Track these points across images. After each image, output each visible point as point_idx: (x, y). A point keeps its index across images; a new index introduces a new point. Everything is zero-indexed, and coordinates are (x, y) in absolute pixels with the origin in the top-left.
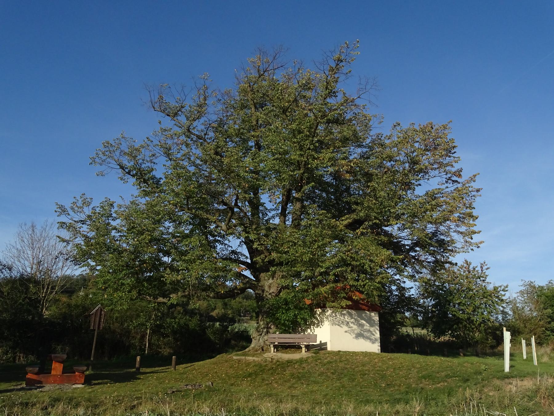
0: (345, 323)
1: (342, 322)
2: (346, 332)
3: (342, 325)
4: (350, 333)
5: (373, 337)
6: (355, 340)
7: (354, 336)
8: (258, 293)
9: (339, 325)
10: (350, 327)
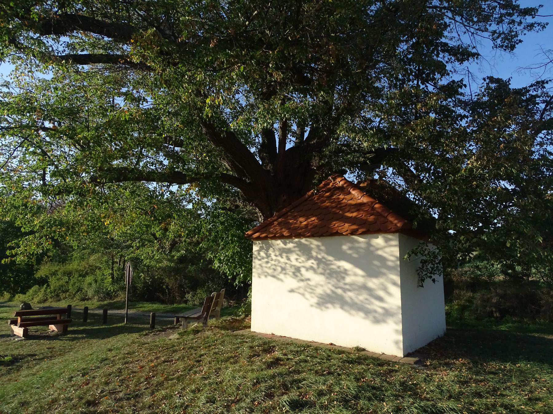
0: (290, 271)
1: (283, 269)
2: (292, 291)
3: (282, 276)
4: (303, 295)
5: (376, 305)
7: (315, 300)
9: (274, 276)
10: (302, 280)
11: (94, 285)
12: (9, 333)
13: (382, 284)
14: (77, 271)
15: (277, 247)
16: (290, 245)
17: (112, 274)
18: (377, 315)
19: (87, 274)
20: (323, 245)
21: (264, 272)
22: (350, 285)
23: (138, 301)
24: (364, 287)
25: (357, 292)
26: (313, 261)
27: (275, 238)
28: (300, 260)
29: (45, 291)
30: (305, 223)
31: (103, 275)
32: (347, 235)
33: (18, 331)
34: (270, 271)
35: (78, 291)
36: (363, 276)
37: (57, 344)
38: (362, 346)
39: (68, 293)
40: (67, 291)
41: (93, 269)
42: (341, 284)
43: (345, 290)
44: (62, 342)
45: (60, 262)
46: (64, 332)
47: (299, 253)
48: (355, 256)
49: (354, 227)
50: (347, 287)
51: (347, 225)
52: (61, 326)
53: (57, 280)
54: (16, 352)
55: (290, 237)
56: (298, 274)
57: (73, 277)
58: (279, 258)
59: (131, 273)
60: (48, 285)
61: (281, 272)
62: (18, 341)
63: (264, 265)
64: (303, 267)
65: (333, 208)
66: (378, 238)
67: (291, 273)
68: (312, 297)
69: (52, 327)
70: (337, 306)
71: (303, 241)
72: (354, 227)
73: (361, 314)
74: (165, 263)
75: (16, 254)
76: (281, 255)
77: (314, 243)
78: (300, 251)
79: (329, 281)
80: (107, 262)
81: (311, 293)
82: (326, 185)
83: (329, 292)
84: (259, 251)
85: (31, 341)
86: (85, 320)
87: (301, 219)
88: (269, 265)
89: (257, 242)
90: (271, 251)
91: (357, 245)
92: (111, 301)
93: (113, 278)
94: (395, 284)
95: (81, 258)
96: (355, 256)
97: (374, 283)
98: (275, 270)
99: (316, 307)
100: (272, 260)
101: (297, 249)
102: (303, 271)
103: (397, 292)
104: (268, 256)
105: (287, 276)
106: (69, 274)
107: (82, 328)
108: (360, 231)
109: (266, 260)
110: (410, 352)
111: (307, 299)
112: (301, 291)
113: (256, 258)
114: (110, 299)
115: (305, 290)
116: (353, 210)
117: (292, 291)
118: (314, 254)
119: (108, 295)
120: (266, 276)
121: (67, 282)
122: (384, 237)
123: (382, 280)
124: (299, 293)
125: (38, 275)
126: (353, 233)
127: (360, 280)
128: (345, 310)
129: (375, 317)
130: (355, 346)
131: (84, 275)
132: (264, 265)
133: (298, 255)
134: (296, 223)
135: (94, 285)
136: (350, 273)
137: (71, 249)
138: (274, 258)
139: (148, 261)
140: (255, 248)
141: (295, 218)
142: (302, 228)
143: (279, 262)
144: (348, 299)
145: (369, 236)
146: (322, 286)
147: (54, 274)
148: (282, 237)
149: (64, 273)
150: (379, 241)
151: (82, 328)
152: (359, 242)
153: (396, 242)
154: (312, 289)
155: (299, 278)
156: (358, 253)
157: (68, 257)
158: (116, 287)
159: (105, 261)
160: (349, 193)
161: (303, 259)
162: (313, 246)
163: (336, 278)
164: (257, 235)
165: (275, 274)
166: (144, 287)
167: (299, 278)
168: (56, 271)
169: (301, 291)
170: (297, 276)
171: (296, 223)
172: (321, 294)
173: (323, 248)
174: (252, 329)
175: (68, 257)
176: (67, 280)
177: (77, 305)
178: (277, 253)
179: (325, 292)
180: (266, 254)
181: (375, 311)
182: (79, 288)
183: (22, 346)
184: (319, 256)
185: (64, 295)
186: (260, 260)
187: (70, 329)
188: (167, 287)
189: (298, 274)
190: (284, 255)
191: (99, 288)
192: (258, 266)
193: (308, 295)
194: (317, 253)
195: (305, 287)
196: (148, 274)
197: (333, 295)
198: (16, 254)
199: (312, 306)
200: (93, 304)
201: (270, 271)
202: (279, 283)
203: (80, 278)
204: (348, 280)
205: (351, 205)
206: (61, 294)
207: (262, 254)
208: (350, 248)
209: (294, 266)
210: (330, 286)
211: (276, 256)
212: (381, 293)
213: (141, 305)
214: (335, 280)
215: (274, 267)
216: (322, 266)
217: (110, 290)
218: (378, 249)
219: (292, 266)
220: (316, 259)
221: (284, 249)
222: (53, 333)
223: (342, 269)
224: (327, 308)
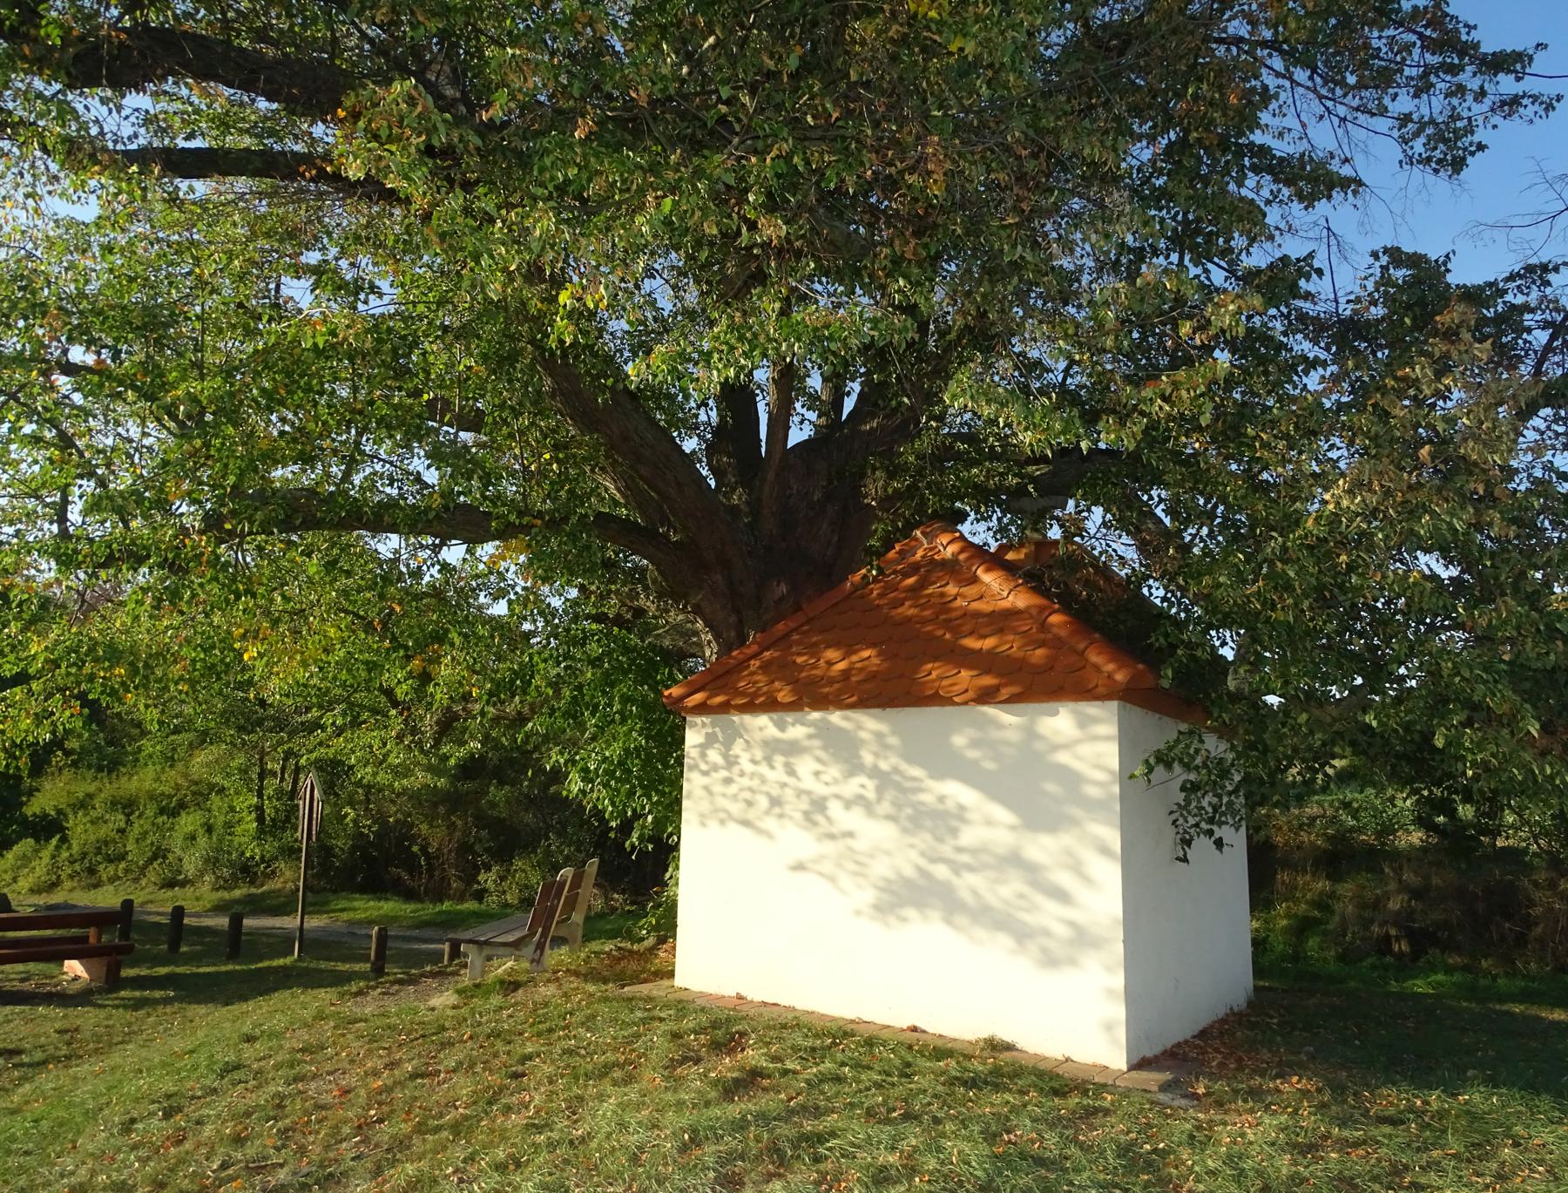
1: (775, 802)
3: (770, 823)
4: (832, 879)
5: (1049, 914)
7: (869, 896)
9: (746, 823)
11: (202, 841)
13: (1069, 853)
14: (152, 796)
15: (758, 736)
17: (259, 809)
18: (1050, 944)
19: (182, 805)
20: (894, 733)
22: (974, 851)
23: (335, 891)
24: (1015, 861)
26: (863, 779)
27: (751, 707)
28: (825, 778)
29: (53, 857)
30: (842, 666)
31: (232, 809)
32: (966, 703)
34: (736, 808)
35: (155, 857)
36: (1013, 828)
37: (87, 1018)
38: (1005, 1035)
39: (123, 865)
40: (122, 857)
41: (201, 794)
42: (946, 850)
43: (957, 868)
44: (102, 1013)
45: (100, 769)
48: (990, 765)
50: (965, 858)
51: (965, 674)
52: (100, 965)
53: (92, 822)
55: (794, 706)
56: (819, 818)
57: (140, 816)
58: (763, 769)
60: (64, 840)
61: (767, 813)
63: (718, 788)
64: (837, 797)
67: (798, 816)
69: (74, 967)
70: (935, 916)
71: (836, 717)
73: (1005, 941)
76: (768, 760)
77: (868, 724)
78: (825, 748)
80: (244, 771)
83: (909, 872)
84: (703, 748)
86: (174, 946)
87: (832, 654)
88: (733, 789)
90: (738, 748)
91: (995, 734)
92: (253, 890)
93: (260, 819)
94: (1105, 850)
95: (167, 759)
96: (990, 765)
98: (749, 803)
100: (742, 774)
102: (835, 808)
103: (1108, 877)
104: (731, 762)
105: (786, 822)
106: (128, 806)
107: (162, 970)
109: (724, 773)
113: (695, 767)
114: (252, 883)
115: (840, 866)
118: (868, 758)
119: (246, 871)
120: (722, 822)
121: (122, 831)
123: (1066, 839)
125: (37, 805)
129: (1044, 950)
131: (171, 810)
132: (718, 788)
133: (819, 760)
134: (813, 666)
135: (202, 841)
137: (136, 731)
138: (748, 767)
140: (693, 738)
143: (764, 781)
144: (965, 895)
146: (888, 853)
147: (83, 804)
148: (771, 705)
149: (114, 804)
151: (162, 970)
152: (1000, 726)
153: (1109, 728)
155: (821, 830)
157: (126, 753)
159: (240, 770)
160: (975, 580)
161: (834, 772)
162: (863, 735)
164: (698, 697)
165: (751, 815)
166: (354, 848)
167: (821, 830)
168: (90, 796)
169: (827, 867)
170: (815, 824)
171: (813, 666)
173: (893, 740)
174: (679, 981)
175: (126, 753)
176: (123, 825)
177: (151, 902)
178: (759, 755)
180: (726, 756)
181: (1047, 933)
182: (159, 848)
184: (884, 766)
185: (111, 869)
186: (706, 773)
188: (424, 849)
189: (819, 818)
190: (779, 760)
191: (218, 850)
192: (699, 792)
193: (845, 880)
194: (876, 755)
196: (367, 809)
199: (858, 913)
200: (198, 899)
201: (736, 808)
203: (160, 820)
206: (101, 867)
207: (714, 756)
208: (974, 744)
209: (808, 793)
210: (913, 855)
211: (754, 762)
212: (1064, 879)
213: (343, 904)
214: (928, 837)
215: (747, 795)
216: (890, 795)
218: (1056, 748)
219: (800, 793)
220: (875, 773)
221: (777, 741)
222: (77, 986)
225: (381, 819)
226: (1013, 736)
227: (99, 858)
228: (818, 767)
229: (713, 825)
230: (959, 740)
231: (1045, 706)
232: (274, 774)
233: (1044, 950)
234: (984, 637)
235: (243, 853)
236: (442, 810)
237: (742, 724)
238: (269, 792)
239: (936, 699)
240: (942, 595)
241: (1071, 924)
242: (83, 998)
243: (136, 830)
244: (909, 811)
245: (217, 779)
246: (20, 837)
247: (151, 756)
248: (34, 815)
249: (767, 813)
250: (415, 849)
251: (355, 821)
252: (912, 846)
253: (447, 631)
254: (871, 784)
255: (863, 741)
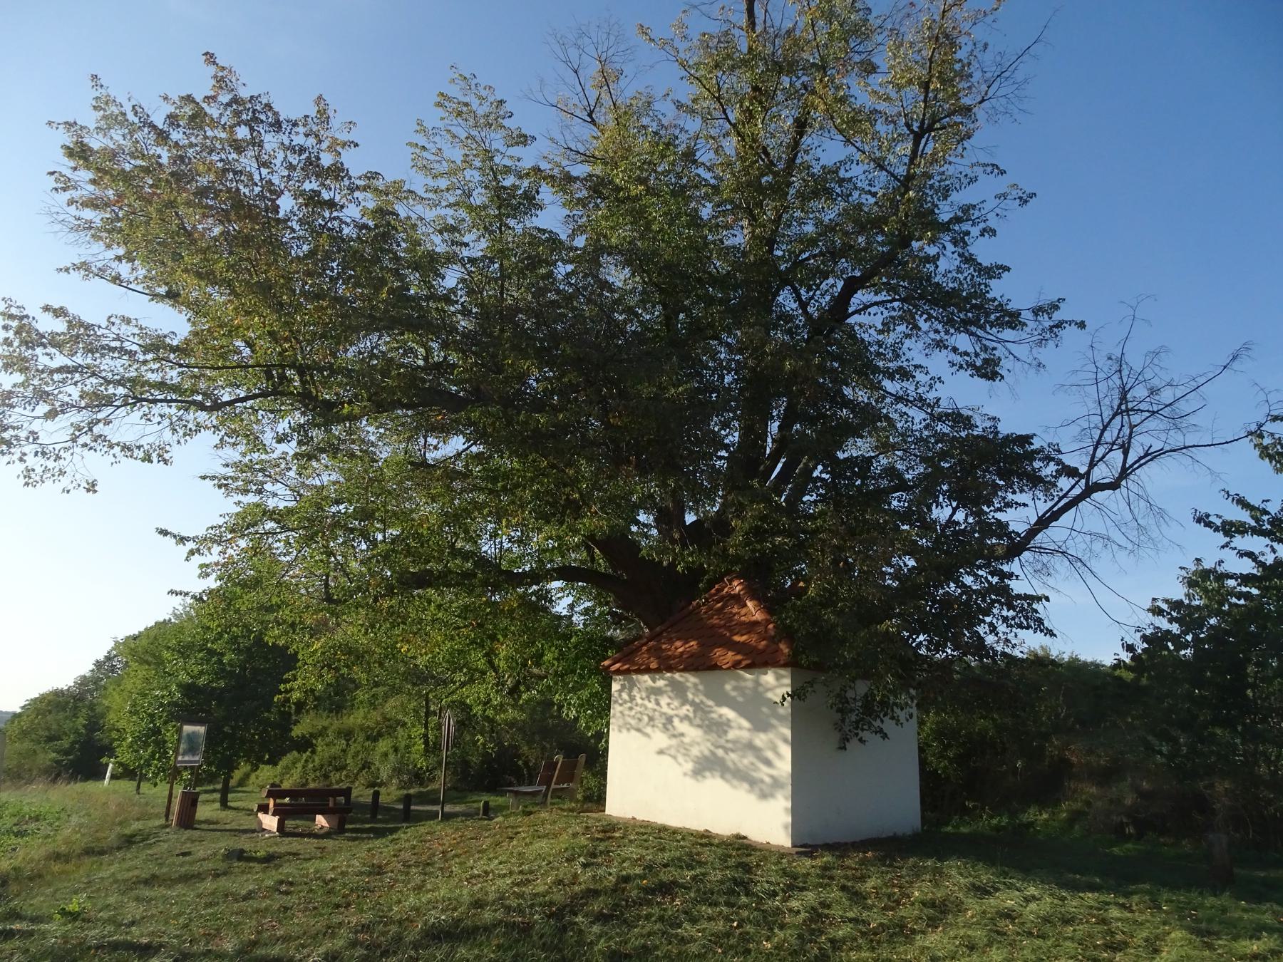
0: (659, 722)
1: (651, 719)
2: (661, 752)
3: (648, 730)
4: (675, 758)
5: (764, 772)
6: (690, 781)
7: (689, 766)
8: (594, 775)
9: (639, 730)
10: (674, 736)
11: (392, 757)
12: (254, 826)
13: (771, 742)
14: (362, 728)
15: (644, 685)
16: (661, 683)
17: (425, 736)
18: (764, 787)
19: (380, 735)
20: (701, 683)
21: (626, 724)
22: (734, 742)
23: (471, 791)
24: (750, 746)
25: (740, 753)
26: (688, 707)
27: (639, 671)
28: (672, 706)
29: (304, 767)
30: (681, 650)
31: (410, 737)
32: (729, 668)
33: (270, 822)
34: (633, 722)
35: (363, 768)
36: (749, 730)
37: (329, 844)
38: (743, 833)
39: (344, 773)
40: (344, 767)
41: (390, 726)
42: (722, 742)
43: (726, 750)
44: (337, 842)
45: (331, 711)
46: (337, 831)
47: (670, 694)
48: (740, 699)
49: (739, 657)
50: (730, 745)
51: (730, 653)
52: (335, 818)
53: (327, 745)
54: (271, 850)
55: (658, 670)
56: (670, 727)
57: (355, 742)
58: (646, 702)
59: (452, 730)
60: (313, 752)
61: (648, 724)
62: (270, 837)
63: (627, 712)
64: (677, 716)
65: (720, 627)
66: (766, 674)
67: (660, 725)
68: (686, 761)
69: (321, 820)
70: (717, 774)
71: (677, 676)
72: (739, 657)
73: (746, 786)
74: (511, 713)
75: (292, 689)
76: (648, 697)
77: (691, 679)
78: (672, 691)
79: (708, 737)
80: (416, 711)
81: (685, 755)
82: (719, 591)
83: (707, 753)
84: (620, 691)
85: (290, 839)
86: (374, 815)
87: (678, 643)
88: (633, 713)
89: (617, 677)
90: (635, 692)
91: (743, 684)
92: (422, 789)
93: (426, 743)
94: (785, 741)
95: (371, 704)
96: (740, 699)
97: (761, 740)
98: (640, 720)
99: (692, 777)
100: (637, 705)
101: (669, 689)
102: (676, 721)
103: (786, 751)
104: (632, 699)
105: (656, 729)
106: (347, 734)
107: (367, 826)
108: (744, 663)
109: (629, 705)
110: (809, 843)
111: (680, 764)
112: (673, 752)
113: (616, 702)
114: (421, 785)
115: (678, 751)
116: (744, 632)
117: (661, 752)
118: (690, 696)
119: (418, 777)
120: (628, 730)
121: (344, 751)
122: (776, 673)
123: (771, 735)
124: (670, 755)
125: (297, 731)
126: (736, 665)
127: (745, 735)
128: (727, 781)
129: (761, 790)
130: (735, 833)
131: (374, 738)
132: (627, 712)
133: (670, 697)
134: (669, 650)
135: (392, 757)
136: (733, 724)
137: (352, 686)
138: (640, 701)
139: (480, 707)
140: (615, 687)
141: (671, 641)
142: (675, 657)
143: (646, 708)
144: (730, 764)
145: (756, 671)
146: (698, 744)
147: (322, 733)
148: (648, 670)
149: (339, 733)
150: (769, 678)
151: (367, 826)
152: (745, 680)
153: (788, 681)
154: (684, 749)
155: (670, 733)
156: (743, 695)
157: (347, 701)
158: (432, 760)
159: (414, 710)
160: (745, 605)
161: (676, 703)
162: (689, 684)
163: (716, 733)
164: (617, 665)
165: (641, 726)
166: (483, 762)
167: (670, 733)
168: (325, 728)
169: (673, 752)
170: (668, 730)
171: (669, 650)
172: (697, 757)
173: (701, 687)
174: (607, 812)
175: (347, 701)
176: (344, 746)
177: (361, 796)
178: (644, 695)
179: (701, 752)
180: (630, 696)
181: (762, 781)
182: (366, 762)
183: (277, 844)
184: (697, 700)
185: (338, 775)
186: (621, 705)
187: (347, 826)
188: (526, 763)
189: (670, 727)
190: (653, 698)
191: (400, 763)
192: (618, 715)
193: (681, 759)
194: (693, 694)
195: (679, 746)
196: (491, 736)
197: (712, 758)
198: (292, 689)
199: (685, 774)
200: (389, 794)
201: (633, 722)
202: (644, 739)
203: (367, 744)
204: (732, 735)
205: (743, 623)
206: (332, 774)
207: (625, 696)
208: (735, 688)
209: (665, 714)
210: (709, 744)
211: (642, 699)
212: (770, 755)
213: (475, 798)
214: (715, 735)
215: (639, 716)
216: (699, 714)
217: (421, 768)
218: (768, 690)
219: (663, 714)
220: (693, 704)
221: (653, 688)
222: (322, 832)
223: (724, 718)
224: (704, 777)
225: (499, 743)
226: (750, 684)
227: (330, 768)
228: (668, 701)
229: (624, 731)
230: (728, 687)
231: (763, 670)
232: (435, 714)
233: (761, 790)
234: (742, 635)
235: (416, 765)
236: (537, 737)
237: (637, 680)
238: (431, 725)
239: (715, 667)
240: (731, 613)
241: (772, 777)
242: (327, 835)
243: (353, 750)
244: (707, 722)
245: (400, 717)
246: (290, 750)
247: (361, 702)
248: (298, 737)
249: (648, 724)
250: (520, 763)
251: (484, 745)
252: (708, 740)
253: (496, 634)
254: (691, 709)
255: (688, 688)
